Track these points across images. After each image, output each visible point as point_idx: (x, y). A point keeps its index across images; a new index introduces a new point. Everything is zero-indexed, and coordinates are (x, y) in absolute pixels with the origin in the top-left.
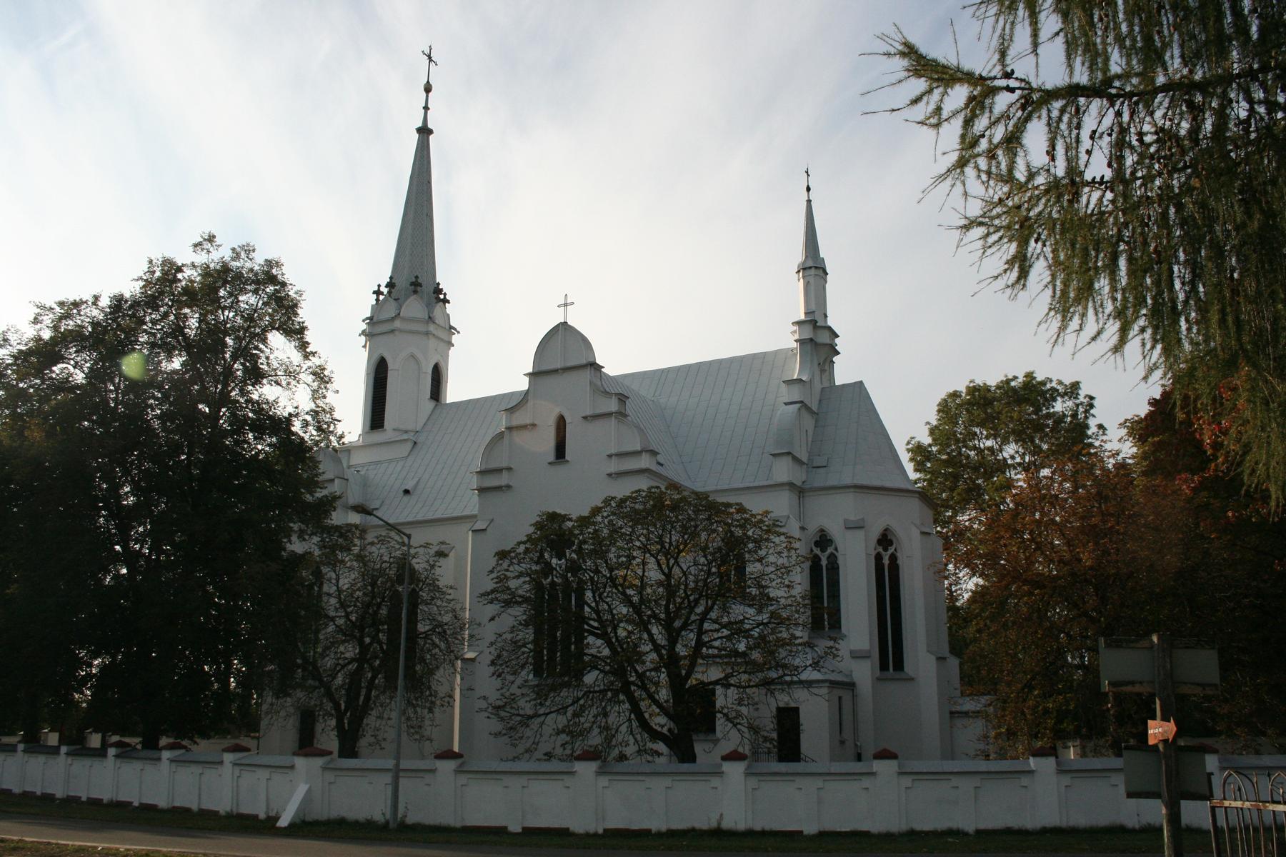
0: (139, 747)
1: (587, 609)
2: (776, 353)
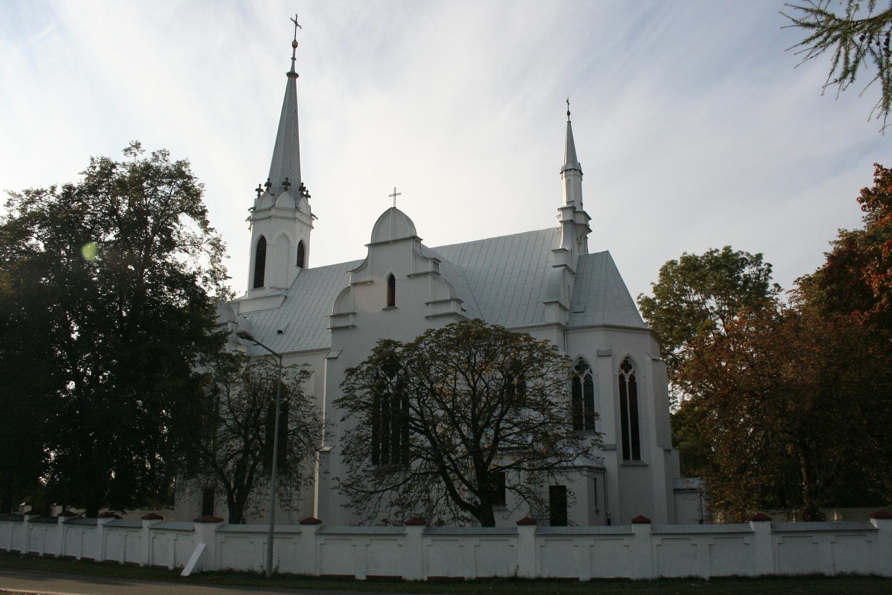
0: (84, 516)
1: (411, 411)
2: (546, 231)
